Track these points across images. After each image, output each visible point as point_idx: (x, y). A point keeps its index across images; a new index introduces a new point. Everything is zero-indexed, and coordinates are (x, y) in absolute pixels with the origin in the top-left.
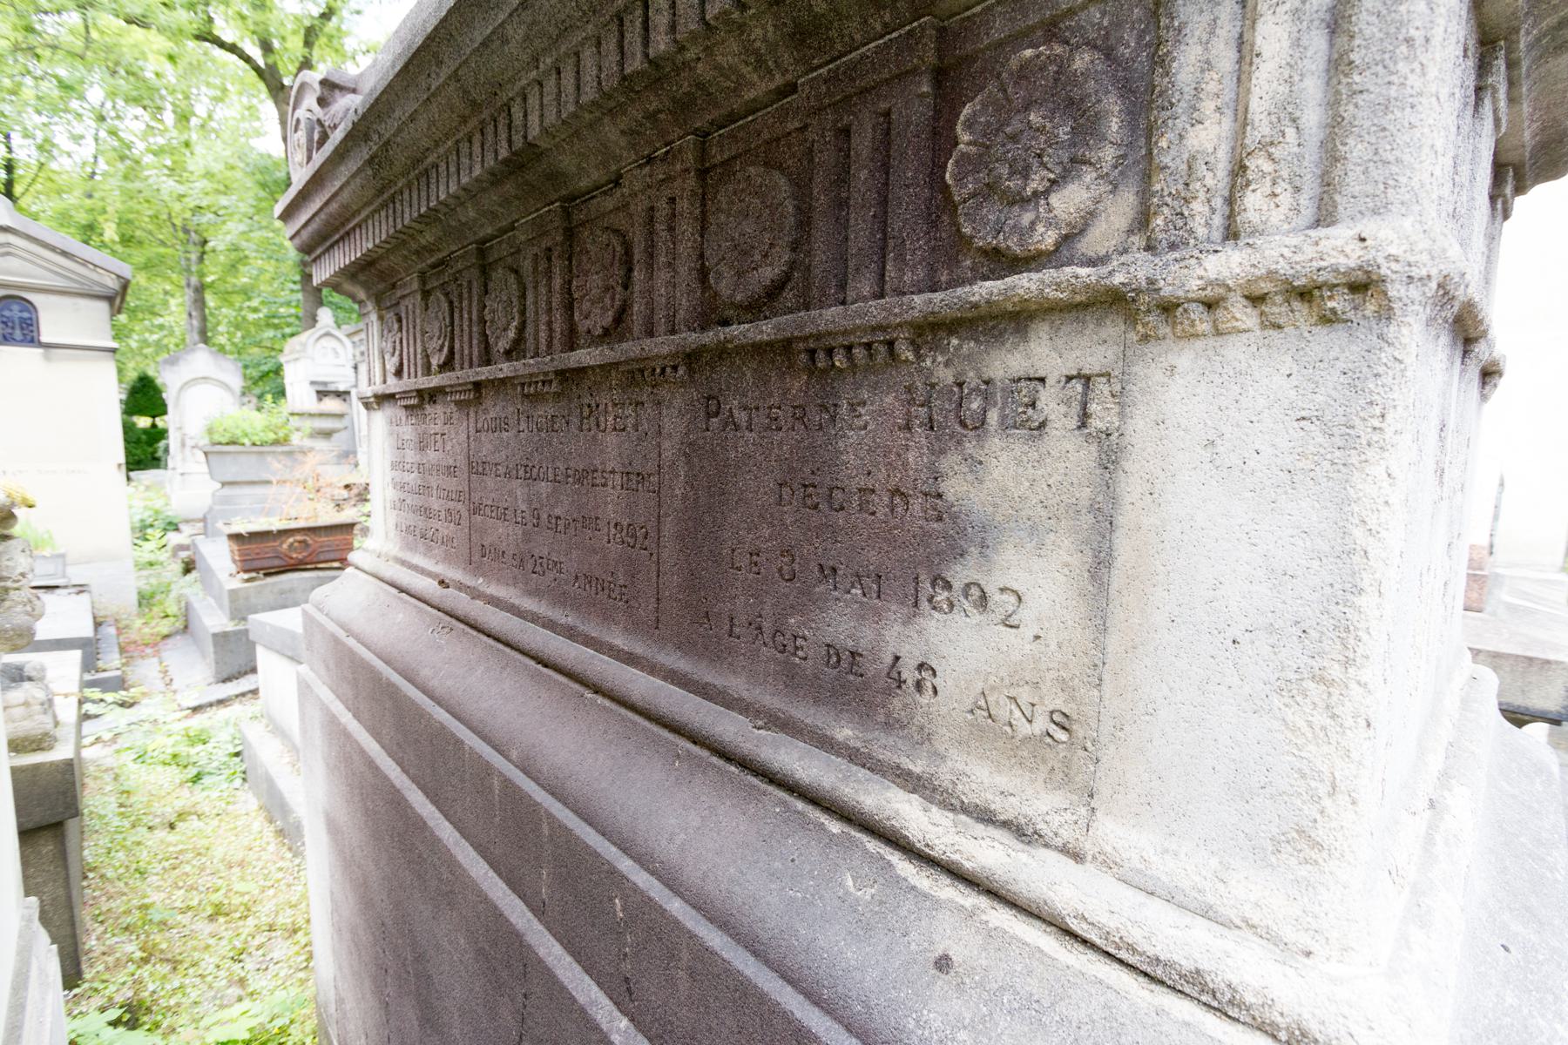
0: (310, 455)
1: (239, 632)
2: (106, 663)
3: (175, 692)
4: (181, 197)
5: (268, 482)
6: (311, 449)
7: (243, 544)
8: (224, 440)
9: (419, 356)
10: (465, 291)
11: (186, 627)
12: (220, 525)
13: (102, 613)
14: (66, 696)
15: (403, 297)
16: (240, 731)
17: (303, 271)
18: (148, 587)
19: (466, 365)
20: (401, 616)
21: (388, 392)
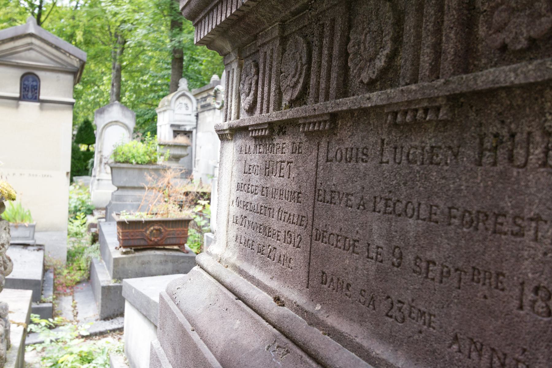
0: (168, 172)
1: (117, 287)
2: (45, 297)
3: (78, 322)
4: (115, 14)
5: (143, 188)
6: (169, 168)
7: (125, 229)
8: (121, 160)
9: (272, 94)
10: (327, 32)
11: (89, 278)
12: (114, 215)
13: (48, 264)
14: (19, 324)
15: (263, 45)
16: (109, 359)
17: (173, 56)
18: (73, 249)
19: (321, 98)
20: (238, 322)
21: (242, 125)
